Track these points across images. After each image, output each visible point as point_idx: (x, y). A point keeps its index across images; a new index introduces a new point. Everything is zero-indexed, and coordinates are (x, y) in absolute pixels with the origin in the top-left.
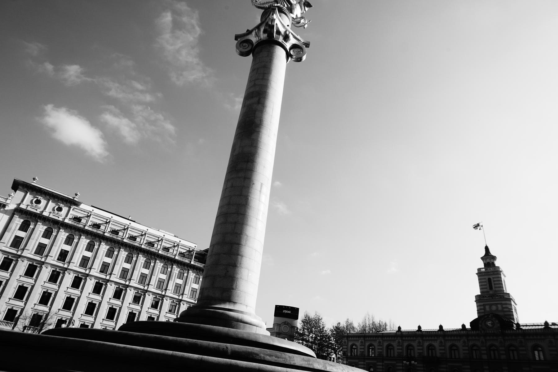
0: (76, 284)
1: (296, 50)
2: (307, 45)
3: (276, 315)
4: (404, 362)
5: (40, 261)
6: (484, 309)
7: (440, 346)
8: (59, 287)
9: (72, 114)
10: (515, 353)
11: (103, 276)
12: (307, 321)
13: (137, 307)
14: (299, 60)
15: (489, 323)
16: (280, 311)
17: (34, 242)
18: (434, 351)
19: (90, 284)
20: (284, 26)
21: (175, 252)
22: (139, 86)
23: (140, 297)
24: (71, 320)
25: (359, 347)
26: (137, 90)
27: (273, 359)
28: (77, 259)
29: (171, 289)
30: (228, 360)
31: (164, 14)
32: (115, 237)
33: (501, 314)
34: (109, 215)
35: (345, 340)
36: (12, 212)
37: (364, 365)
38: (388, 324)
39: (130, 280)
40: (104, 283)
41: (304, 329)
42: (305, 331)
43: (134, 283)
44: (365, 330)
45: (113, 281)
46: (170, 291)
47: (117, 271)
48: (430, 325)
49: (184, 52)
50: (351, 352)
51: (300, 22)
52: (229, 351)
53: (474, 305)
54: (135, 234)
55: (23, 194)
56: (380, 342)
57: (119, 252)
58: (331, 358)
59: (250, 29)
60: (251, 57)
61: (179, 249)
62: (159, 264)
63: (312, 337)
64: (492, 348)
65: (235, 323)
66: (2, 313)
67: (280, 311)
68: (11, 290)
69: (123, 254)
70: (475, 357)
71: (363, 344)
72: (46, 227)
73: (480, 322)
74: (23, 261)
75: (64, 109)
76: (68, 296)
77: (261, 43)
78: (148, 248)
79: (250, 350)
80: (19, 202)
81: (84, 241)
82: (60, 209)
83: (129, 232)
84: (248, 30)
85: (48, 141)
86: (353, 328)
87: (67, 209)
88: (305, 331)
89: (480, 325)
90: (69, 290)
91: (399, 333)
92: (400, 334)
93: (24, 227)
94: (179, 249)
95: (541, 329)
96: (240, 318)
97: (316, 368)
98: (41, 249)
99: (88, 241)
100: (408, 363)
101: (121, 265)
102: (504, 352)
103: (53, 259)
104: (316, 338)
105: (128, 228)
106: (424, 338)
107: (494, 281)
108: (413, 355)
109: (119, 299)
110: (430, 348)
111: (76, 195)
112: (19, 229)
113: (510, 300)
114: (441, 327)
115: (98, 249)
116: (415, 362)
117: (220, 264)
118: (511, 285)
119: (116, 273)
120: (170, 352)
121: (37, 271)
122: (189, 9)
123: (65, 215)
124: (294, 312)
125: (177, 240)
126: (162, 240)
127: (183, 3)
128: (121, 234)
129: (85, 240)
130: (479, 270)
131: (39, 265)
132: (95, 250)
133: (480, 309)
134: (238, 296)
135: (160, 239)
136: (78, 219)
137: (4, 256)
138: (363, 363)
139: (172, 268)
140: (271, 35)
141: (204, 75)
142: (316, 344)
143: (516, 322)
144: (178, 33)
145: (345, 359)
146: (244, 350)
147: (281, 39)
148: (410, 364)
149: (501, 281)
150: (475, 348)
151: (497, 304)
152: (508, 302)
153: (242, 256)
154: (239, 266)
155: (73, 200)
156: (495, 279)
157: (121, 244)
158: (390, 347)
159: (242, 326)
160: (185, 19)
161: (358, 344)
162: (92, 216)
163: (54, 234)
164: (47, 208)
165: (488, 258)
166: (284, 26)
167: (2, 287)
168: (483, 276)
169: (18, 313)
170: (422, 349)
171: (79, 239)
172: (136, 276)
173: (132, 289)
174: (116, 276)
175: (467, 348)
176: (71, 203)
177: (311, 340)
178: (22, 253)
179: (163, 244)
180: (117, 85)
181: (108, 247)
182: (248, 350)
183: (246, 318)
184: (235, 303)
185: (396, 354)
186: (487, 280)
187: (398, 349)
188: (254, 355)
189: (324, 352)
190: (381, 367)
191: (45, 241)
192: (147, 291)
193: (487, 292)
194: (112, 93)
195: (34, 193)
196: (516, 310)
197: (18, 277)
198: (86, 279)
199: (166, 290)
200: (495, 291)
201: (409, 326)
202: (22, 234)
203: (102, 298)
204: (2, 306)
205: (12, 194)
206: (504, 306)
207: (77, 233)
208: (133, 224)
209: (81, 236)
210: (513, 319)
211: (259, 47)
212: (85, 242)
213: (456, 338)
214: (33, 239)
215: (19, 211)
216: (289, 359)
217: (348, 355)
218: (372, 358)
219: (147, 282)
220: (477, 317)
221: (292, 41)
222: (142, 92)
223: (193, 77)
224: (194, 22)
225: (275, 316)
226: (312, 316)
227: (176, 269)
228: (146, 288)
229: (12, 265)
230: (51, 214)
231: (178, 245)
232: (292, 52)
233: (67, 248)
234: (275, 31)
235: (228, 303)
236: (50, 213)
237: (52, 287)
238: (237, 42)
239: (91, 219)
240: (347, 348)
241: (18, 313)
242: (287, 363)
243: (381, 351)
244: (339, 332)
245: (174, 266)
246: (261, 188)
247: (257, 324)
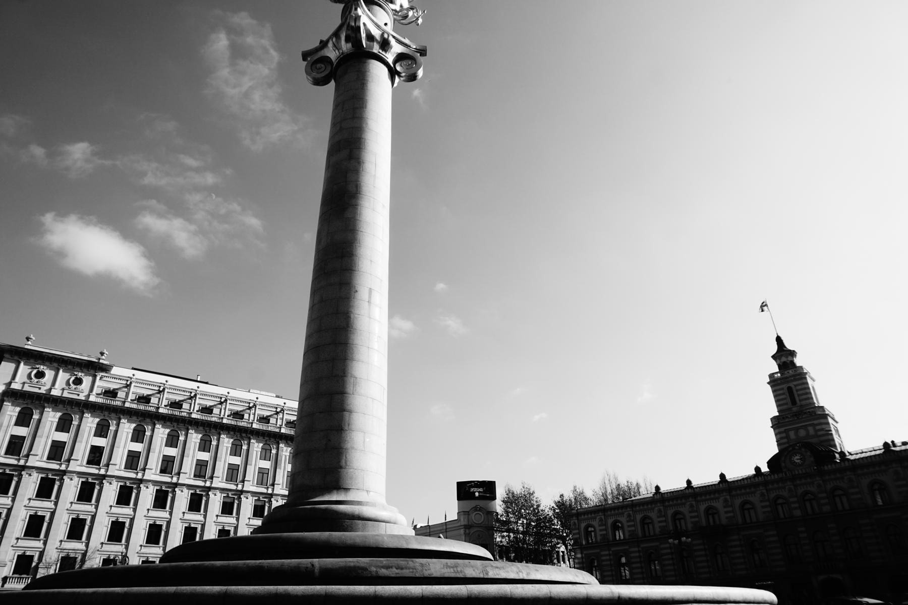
0: (124, 497)
1: (404, 63)
2: (423, 52)
3: (459, 498)
4: (671, 541)
6: (788, 437)
8: (97, 508)
9: (88, 223)
10: (844, 499)
11: (166, 478)
12: (511, 501)
13: (230, 520)
14: (412, 78)
15: (797, 459)
16: (464, 490)
17: (43, 440)
18: (716, 516)
19: (147, 495)
20: (378, 26)
21: (279, 422)
22: (191, 162)
23: (233, 504)
24: (125, 557)
25: (598, 528)
26: (190, 169)
27: (393, 572)
28: (120, 457)
29: (281, 482)
30: (271, 587)
31: (213, 36)
32: (177, 413)
33: (814, 440)
34: (161, 379)
35: (574, 520)
37: (610, 555)
38: (642, 484)
40: (170, 490)
41: (507, 512)
42: (511, 515)
43: (219, 482)
44: (606, 500)
45: (184, 485)
46: (280, 486)
47: (189, 466)
49: (257, 96)
52: (317, 571)
54: (209, 404)
55: (12, 366)
56: (629, 516)
57: (186, 435)
58: (558, 552)
60: (332, 84)
61: (286, 417)
62: (256, 444)
64: (807, 498)
66: (9, 564)
67: (464, 490)
69: (195, 438)
70: (782, 516)
71: (603, 523)
73: (783, 459)
74: (30, 475)
75: (73, 217)
77: (345, 59)
78: (233, 423)
79: (352, 564)
80: (8, 380)
81: (127, 428)
82: (78, 381)
83: (198, 401)
84: (321, 42)
86: (586, 499)
88: (511, 515)
89: (783, 464)
90: (114, 510)
91: (658, 496)
92: (660, 498)
94: (286, 417)
95: (879, 455)
96: (357, 513)
97: (468, 576)
98: (56, 451)
99: (134, 425)
100: (676, 542)
101: (193, 457)
103: (79, 463)
104: (529, 525)
105: (195, 395)
107: (797, 391)
108: (684, 528)
111: (102, 354)
112: (16, 425)
113: (825, 416)
114: (722, 476)
115: (152, 436)
116: (687, 538)
118: (824, 394)
119: (188, 471)
120: (172, 589)
122: (254, 22)
123: (90, 389)
124: (489, 488)
125: (280, 402)
126: (255, 406)
127: (244, 14)
128: (185, 406)
129: (127, 425)
131: (57, 478)
133: (781, 438)
134: (351, 478)
135: (251, 405)
136: (112, 393)
138: (607, 553)
139: (278, 449)
140: (357, 42)
141: (296, 128)
142: (530, 535)
143: (839, 450)
144: (243, 64)
145: (578, 551)
146: (342, 564)
147: (376, 49)
149: (809, 388)
150: (780, 501)
152: (823, 421)
153: (350, 412)
154: (346, 428)
155: (99, 363)
157: (189, 423)
159: (360, 526)
160: (250, 40)
162: (133, 385)
164: (57, 383)
166: (378, 26)
168: (779, 385)
169: (36, 559)
171: (118, 425)
172: (221, 470)
173: (218, 492)
174: (187, 476)
175: (767, 503)
176: (95, 368)
177: (521, 528)
178: (26, 461)
179: (258, 412)
180: (154, 165)
181: (168, 430)
182: (349, 564)
183: (367, 511)
184: (347, 490)
185: (658, 530)
186: (786, 391)
187: (660, 522)
188: (360, 571)
191: (62, 437)
192: (242, 492)
193: (789, 409)
194: (149, 180)
195: (32, 361)
196: (837, 431)
197: (26, 502)
199: (273, 485)
200: (801, 406)
203: (171, 514)
204: (7, 552)
206: (818, 427)
207: (113, 415)
208: (204, 388)
209: (120, 419)
210: (835, 446)
211: (341, 67)
212: (129, 428)
213: (748, 490)
214: (41, 437)
216: (420, 568)
218: (621, 542)
219: (240, 477)
221: (396, 48)
222: (197, 170)
223: (278, 134)
224: (265, 42)
225: (459, 498)
226: (518, 490)
227: (285, 448)
228: (240, 487)
229: (14, 483)
230: (65, 392)
231: (282, 410)
232: (398, 68)
233: (100, 442)
234: (363, 35)
235: (335, 492)
236: (63, 389)
237: (85, 509)
238: (306, 63)
239: (132, 389)
240: (579, 533)
241: (36, 559)
244: (564, 509)
245: (281, 445)
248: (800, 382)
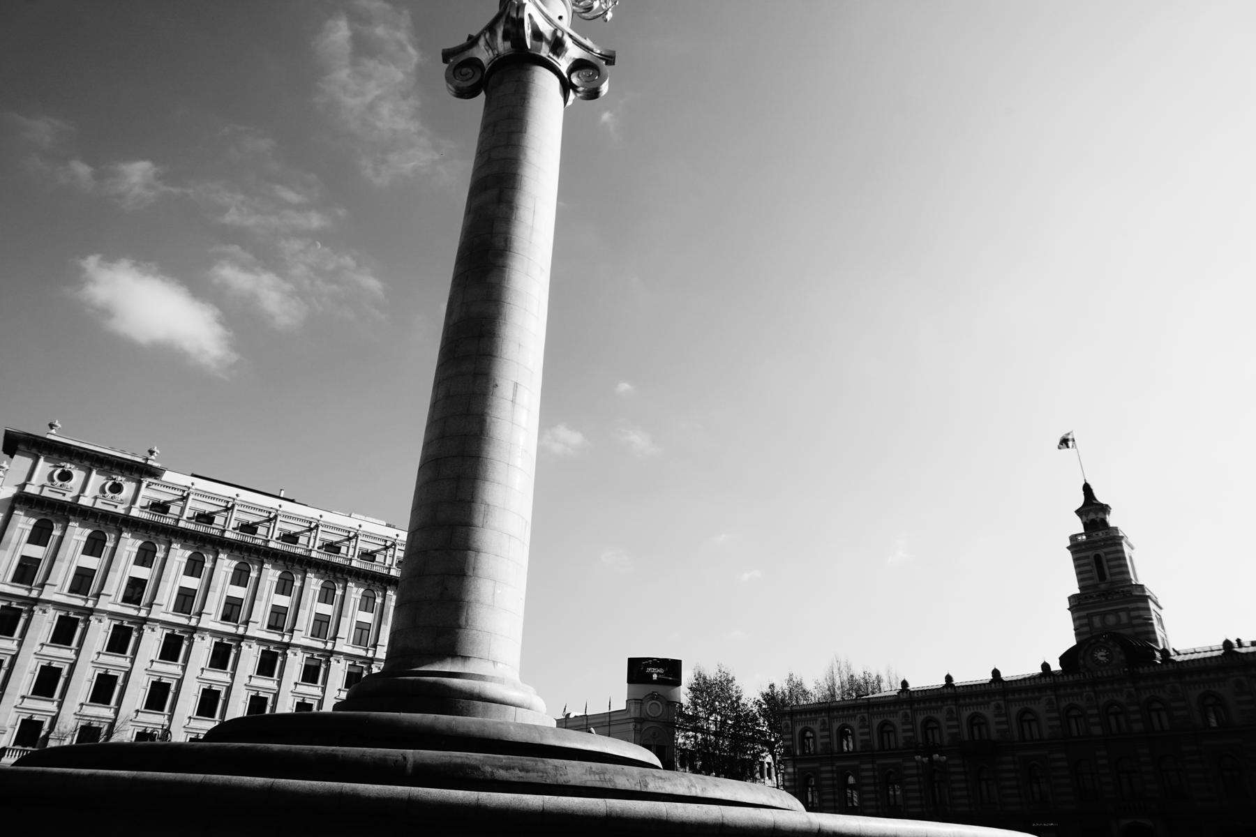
0: (171, 650)
2: (610, 59)
4: (918, 758)
5: (83, 608)
6: (1090, 624)
7: (996, 716)
9: (146, 272)
11: (229, 628)
12: (702, 688)
14: (593, 94)
15: (1101, 655)
16: (638, 670)
17: (65, 565)
19: (202, 649)
20: (549, 20)
21: (389, 561)
22: (291, 196)
23: (318, 668)
25: (818, 734)
26: (288, 205)
27: (514, 776)
32: (249, 540)
35: (787, 721)
36: (9, 504)
37: (832, 772)
38: (885, 678)
39: (292, 631)
41: (695, 704)
43: (302, 637)
44: (833, 696)
45: (253, 638)
47: (261, 614)
48: (972, 672)
49: (385, 110)
50: (803, 746)
51: (591, 8)
53: (1068, 616)
56: (863, 719)
57: (260, 571)
58: (762, 763)
59: (475, 34)
60: (482, 96)
62: (355, 589)
63: (715, 721)
65: (463, 703)
66: (9, 730)
67: (638, 670)
68: (24, 678)
70: (1075, 733)
71: (826, 727)
72: (88, 531)
74: (44, 612)
75: (125, 263)
76: (155, 679)
77: (501, 63)
79: (459, 761)
80: (22, 481)
81: (180, 555)
84: (470, 37)
85: (97, 341)
86: (805, 693)
87: (134, 485)
90: (156, 666)
91: (905, 695)
92: (907, 698)
93: (39, 536)
95: (1216, 657)
96: (477, 690)
97: (620, 787)
98: (82, 580)
99: (189, 553)
100: (926, 760)
101: (268, 600)
102: (1138, 716)
103: (112, 599)
104: (723, 723)
106: (961, 702)
107: (1108, 561)
108: (938, 741)
109: (272, 675)
110: (976, 721)
111: (151, 452)
113: (1145, 598)
117: (435, 578)
118: (1145, 567)
119: (260, 620)
121: (133, 640)
122: (387, 6)
123: (135, 499)
124: (672, 668)
126: (356, 536)
128: (261, 530)
130: (1073, 538)
131: (81, 618)
132: (205, 573)
133: (1081, 626)
135: (351, 535)
136: (161, 507)
137: (59, 614)
144: (369, 64)
145: (790, 764)
146: (447, 760)
147: (545, 52)
148: (931, 760)
149: (1124, 559)
150: (1074, 713)
151: (1115, 612)
152: (1141, 605)
153: (478, 551)
155: (146, 464)
156: (1110, 556)
157: (265, 554)
158: (888, 728)
160: (380, 31)
161: (816, 727)
162: (191, 497)
163: (110, 544)
164: (89, 489)
165: (1092, 510)
166: (549, 20)
167: (3, 671)
169: (46, 726)
170: (957, 726)
171: (167, 551)
172: (305, 621)
173: (299, 651)
174: (258, 626)
175: (1056, 715)
176: (142, 471)
177: (713, 727)
179: (360, 545)
180: (240, 197)
181: (235, 563)
182: (455, 760)
183: (491, 689)
184: (466, 658)
185: (901, 742)
186: (1092, 560)
187: (905, 731)
188: (469, 771)
189: (745, 753)
190: (870, 774)
191: (91, 562)
192: (332, 653)
193: (1095, 586)
194: (232, 217)
195: (56, 456)
196: (1160, 620)
197: (37, 648)
198: (191, 640)
200: (1112, 582)
201: (925, 677)
202: (36, 551)
203: (233, 677)
205: (5, 464)
206: (1133, 614)
207: (161, 537)
208: (288, 507)
209: (170, 543)
210: (1156, 641)
211: (494, 73)
212: (182, 556)
214: (62, 561)
215: (23, 500)
216: (553, 772)
217: (795, 754)
219: (331, 633)
220: (1074, 643)
221: (574, 52)
222: (299, 208)
224: (402, 36)
226: (711, 674)
228: (329, 646)
232: (575, 80)
233: (142, 573)
235: (449, 660)
236: (96, 498)
237: (116, 662)
239: (190, 503)
240: (792, 739)
241: (46, 726)
242: (548, 781)
243: (867, 737)
246: (515, 394)
247: (518, 702)
248: (1113, 549)
